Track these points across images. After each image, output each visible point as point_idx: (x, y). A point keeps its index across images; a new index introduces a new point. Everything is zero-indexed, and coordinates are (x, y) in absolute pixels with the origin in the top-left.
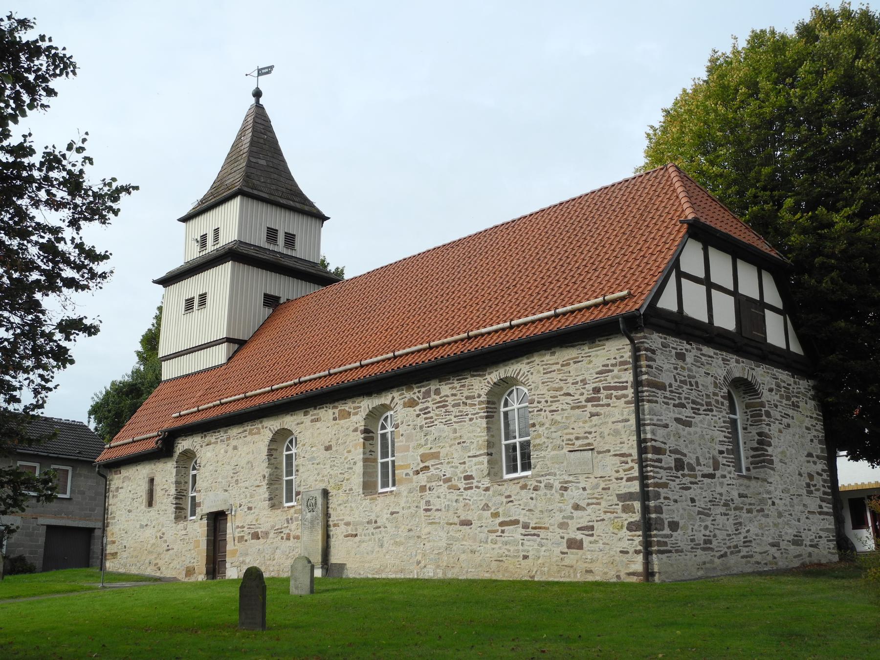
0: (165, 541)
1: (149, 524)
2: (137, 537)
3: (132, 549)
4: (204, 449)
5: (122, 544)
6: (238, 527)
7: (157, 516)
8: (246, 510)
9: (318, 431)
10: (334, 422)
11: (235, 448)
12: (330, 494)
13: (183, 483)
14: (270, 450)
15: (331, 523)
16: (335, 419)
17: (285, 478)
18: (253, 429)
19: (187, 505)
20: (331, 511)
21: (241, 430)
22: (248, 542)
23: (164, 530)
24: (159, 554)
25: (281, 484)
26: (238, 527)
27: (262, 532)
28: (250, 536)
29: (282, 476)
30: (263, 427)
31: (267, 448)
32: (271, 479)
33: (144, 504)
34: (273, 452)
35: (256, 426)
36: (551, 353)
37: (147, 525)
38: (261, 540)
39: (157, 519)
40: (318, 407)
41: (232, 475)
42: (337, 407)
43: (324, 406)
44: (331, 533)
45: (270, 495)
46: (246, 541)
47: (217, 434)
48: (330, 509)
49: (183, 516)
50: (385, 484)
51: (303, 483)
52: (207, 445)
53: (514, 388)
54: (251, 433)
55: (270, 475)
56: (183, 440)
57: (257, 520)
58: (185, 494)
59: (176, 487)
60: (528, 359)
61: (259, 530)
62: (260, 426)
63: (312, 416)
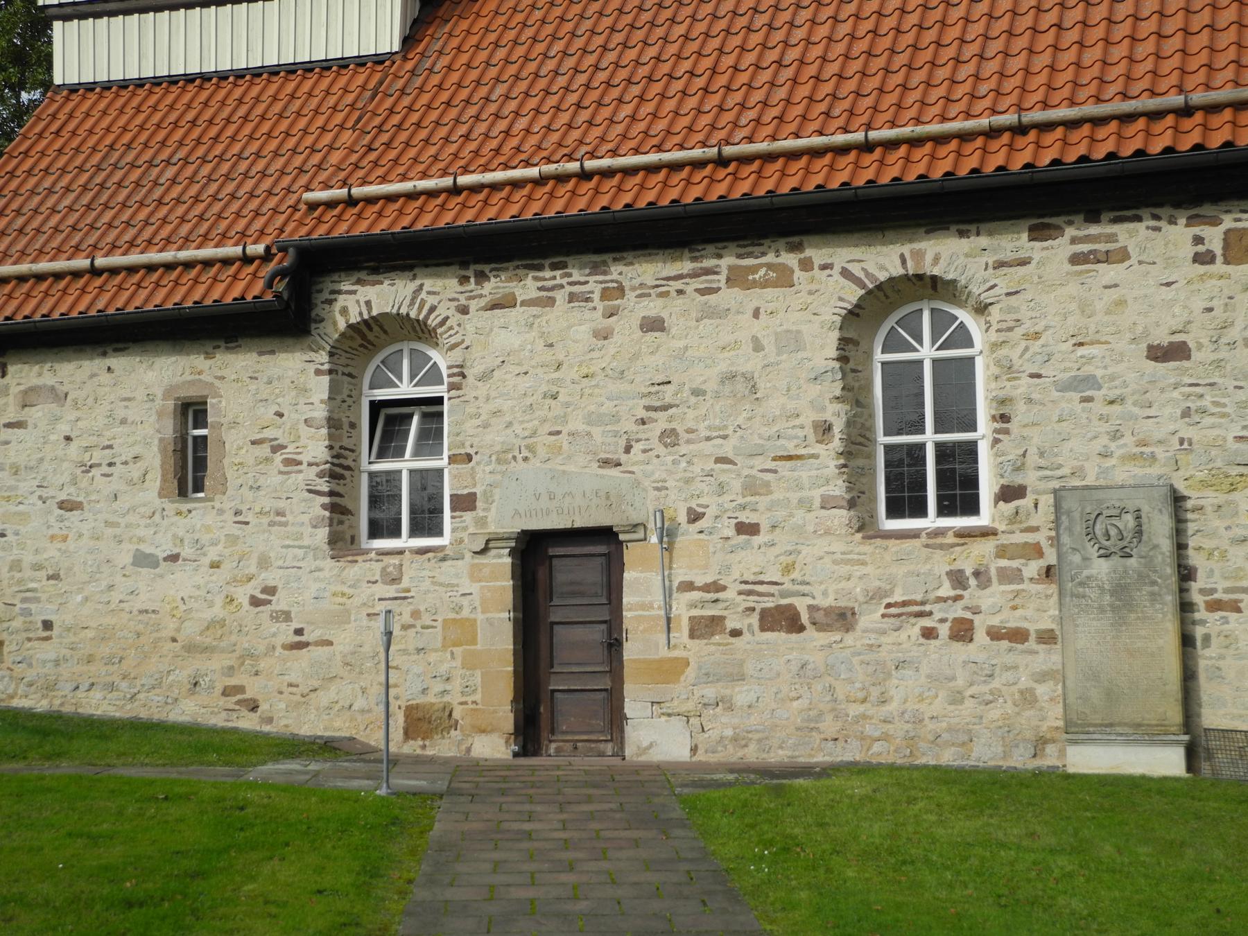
0: (287, 616)
1: (187, 552)
2: (116, 596)
3: (90, 634)
4: (477, 320)
5: (27, 613)
6: (688, 586)
7: (236, 530)
8: (730, 532)
9: (1114, 294)
10: (1201, 269)
11: (654, 325)
12: (1189, 504)
13: (346, 427)
14: (844, 342)
15: (1197, 598)
16: (1203, 258)
17: (883, 439)
18: (754, 269)
19: (357, 499)
20: (1195, 559)
21: (686, 266)
22: (747, 636)
23: (271, 577)
24: (249, 655)
25: (871, 456)
26: (688, 586)
27: (812, 608)
28: (754, 620)
29: (872, 429)
30: (806, 265)
31: (835, 335)
32: (849, 435)
33: (155, 481)
34: (851, 351)
35: (770, 258)
36: (1032, 229)
37: (174, 558)
38: (811, 632)
39: (232, 540)
40: (1105, 216)
41: (642, 413)
42: (1215, 222)
43: (1145, 213)
44: (1199, 632)
45: (849, 490)
46: (736, 633)
47: (547, 274)
48: (1190, 552)
49: (348, 537)
50: (376, 531)
51: (1033, 459)
52: (494, 306)
53: (406, 347)
54: (737, 279)
55: (849, 424)
56: (359, 282)
57: (788, 569)
58: (349, 462)
59: (331, 437)
60: (740, 256)
61: (801, 604)
62: (790, 259)
63: (1074, 241)
